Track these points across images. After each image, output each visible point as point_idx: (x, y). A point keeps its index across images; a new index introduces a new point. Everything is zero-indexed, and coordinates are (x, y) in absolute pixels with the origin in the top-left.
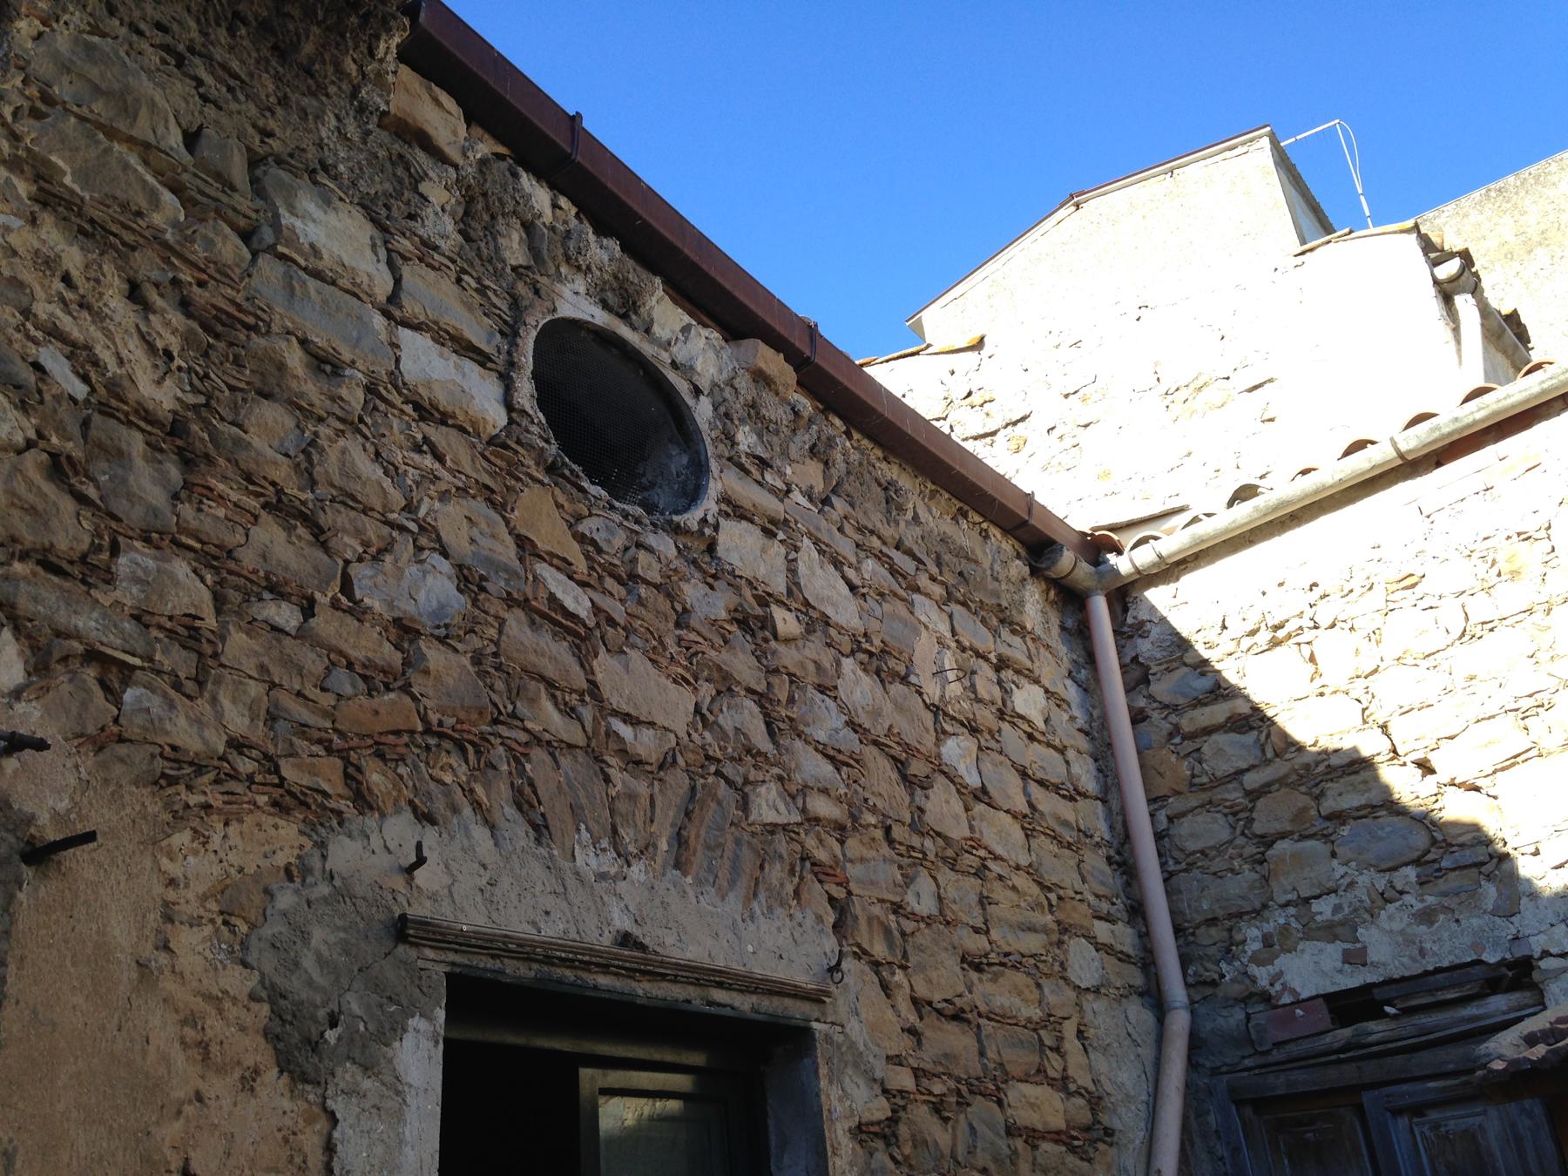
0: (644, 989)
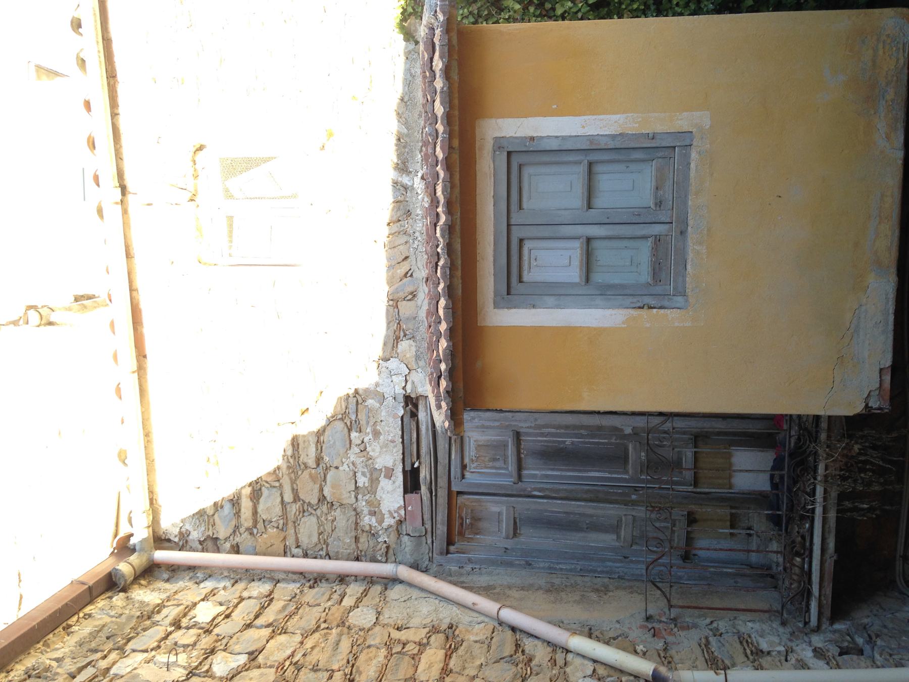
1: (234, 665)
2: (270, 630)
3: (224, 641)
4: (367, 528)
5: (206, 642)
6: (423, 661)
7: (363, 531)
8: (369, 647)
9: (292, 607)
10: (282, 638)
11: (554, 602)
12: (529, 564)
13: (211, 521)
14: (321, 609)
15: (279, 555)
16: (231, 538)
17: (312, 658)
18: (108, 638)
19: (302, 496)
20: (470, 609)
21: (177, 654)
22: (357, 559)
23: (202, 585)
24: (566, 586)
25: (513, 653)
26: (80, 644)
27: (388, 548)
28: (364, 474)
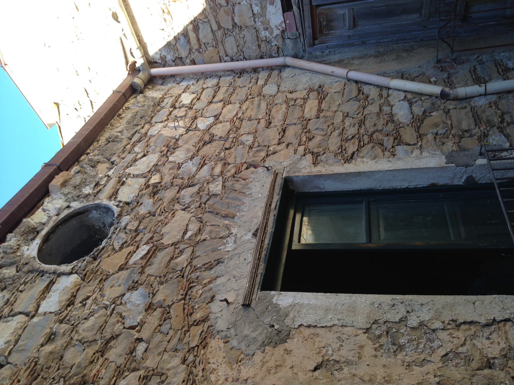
0: (270, 229)
1: (208, 123)
2: (222, 103)
3: (200, 112)
4: (264, 38)
5: (191, 113)
6: (306, 107)
7: (262, 41)
8: (276, 104)
9: (231, 90)
10: (229, 107)
11: (380, 63)
12: (364, 43)
13: (176, 48)
14: (246, 88)
15: (217, 62)
16: (189, 56)
17: (248, 114)
18: (141, 118)
19: (222, 25)
20: (330, 75)
21: (178, 122)
22: (262, 58)
23: (181, 84)
24: (387, 51)
25: (357, 95)
26: (129, 123)
27: (278, 48)
28: (256, 5)
